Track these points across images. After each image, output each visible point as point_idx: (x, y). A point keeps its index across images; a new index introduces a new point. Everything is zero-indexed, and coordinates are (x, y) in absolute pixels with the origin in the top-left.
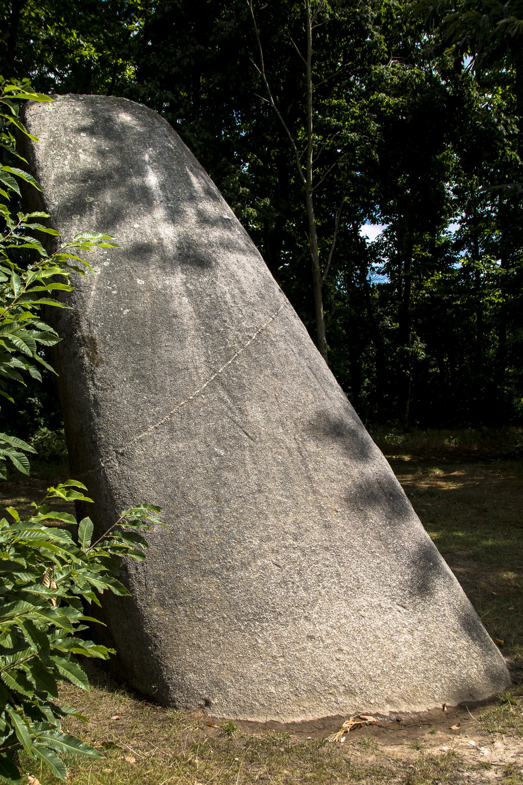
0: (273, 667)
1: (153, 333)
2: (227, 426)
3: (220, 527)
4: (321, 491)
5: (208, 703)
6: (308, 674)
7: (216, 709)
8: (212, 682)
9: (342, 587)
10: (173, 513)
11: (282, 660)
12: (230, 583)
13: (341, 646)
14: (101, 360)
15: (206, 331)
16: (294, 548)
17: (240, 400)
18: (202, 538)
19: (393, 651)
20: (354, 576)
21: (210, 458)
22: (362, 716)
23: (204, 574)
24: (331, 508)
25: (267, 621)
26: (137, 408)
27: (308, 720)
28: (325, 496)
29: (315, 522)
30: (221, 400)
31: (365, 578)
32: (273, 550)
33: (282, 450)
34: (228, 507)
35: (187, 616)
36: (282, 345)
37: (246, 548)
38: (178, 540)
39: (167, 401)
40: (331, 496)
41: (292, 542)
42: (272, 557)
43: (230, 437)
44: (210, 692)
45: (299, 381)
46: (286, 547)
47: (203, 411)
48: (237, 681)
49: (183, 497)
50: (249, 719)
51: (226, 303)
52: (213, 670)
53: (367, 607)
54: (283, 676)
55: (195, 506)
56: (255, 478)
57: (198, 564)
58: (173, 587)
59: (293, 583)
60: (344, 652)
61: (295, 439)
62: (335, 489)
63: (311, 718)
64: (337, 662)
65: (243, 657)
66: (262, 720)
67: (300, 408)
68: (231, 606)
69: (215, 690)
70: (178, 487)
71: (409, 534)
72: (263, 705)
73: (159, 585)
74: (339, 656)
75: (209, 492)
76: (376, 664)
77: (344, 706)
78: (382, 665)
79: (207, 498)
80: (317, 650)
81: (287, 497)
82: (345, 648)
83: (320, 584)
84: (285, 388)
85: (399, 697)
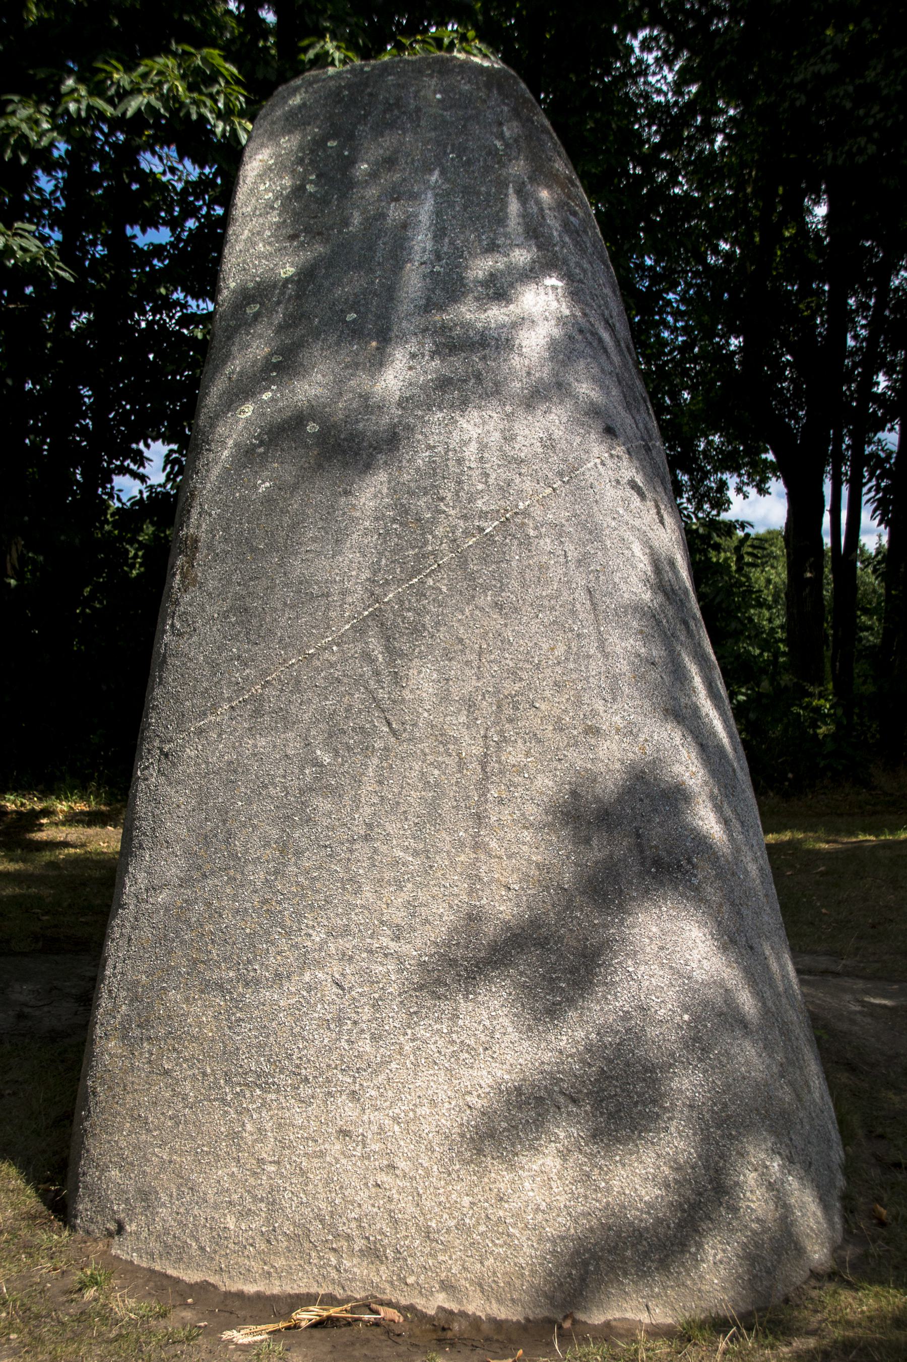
0: (252, 1181)
1: (294, 527)
2: (358, 705)
3: (265, 902)
4: (493, 844)
5: (121, 1229)
6: (307, 1205)
7: (128, 1243)
8: (139, 1191)
9: (453, 1042)
10: (199, 868)
11: (272, 1168)
12: (241, 1010)
13: (396, 1159)
14: (195, 580)
15: (394, 520)
16: (386, 955)
17: (402, 655)
18: (228, 918)
19: (502, 1186)
20: (487, 1023)
21: (302, 769)
22: (374, 1306)
23: (206, 987)
24: (498, 880)
25: (278, 1091)
26: (214, 666)
27: (268, 1293)
28: (496, 857)
29: (451, 907)
30: (367, 657)
31: (510, 1030)
32: (344, 954)
33: (446, 760)
34: (296, 864)
35: (150, 1062)
36: (547, 544)
37: (296, 946)
38: (187, 921)
39: (267, 658)
40: (509, 857)
41: (385, 941)
42: (336, 969)
43: (354, 729)
44: (130, 1210)
45: (547, 617)
46: (370, 952)
47: (325, 678)
48: (180, 1196)
49: (227, 841)
50: (170, 1272)
51: (460, 461)
52: (148, 1170)
53: (488, 1090)
54: (262, 1200)
55: (239, 859)
56: (368, 810)
57: (202, 967)
58: (150, 1005)
59: (355, 1023)
60: (397, 1172)
61: (486, 737)
62: (524, 843)
63: (276, 1290)
64: (373, 1190)
65: (208, 1153)
66: (192, 1276)
67: (525, 675)
68: (224, 1053)
69: (139, 1206)
70: (224, 822)
71: (662, 948)
72: (202, 1249)
73: (131, 1000)
74: (382, 1177)
75: (274, 833)
76: (454, 1207)
77: (349, 1279)
78: (465, 1210)
79: (267, 845)
80: (344, 1161)
81: (416, 853)
82: (402, 1164)
83: (409, 1031)
84: (508, 634)
85: (472, 1282)
